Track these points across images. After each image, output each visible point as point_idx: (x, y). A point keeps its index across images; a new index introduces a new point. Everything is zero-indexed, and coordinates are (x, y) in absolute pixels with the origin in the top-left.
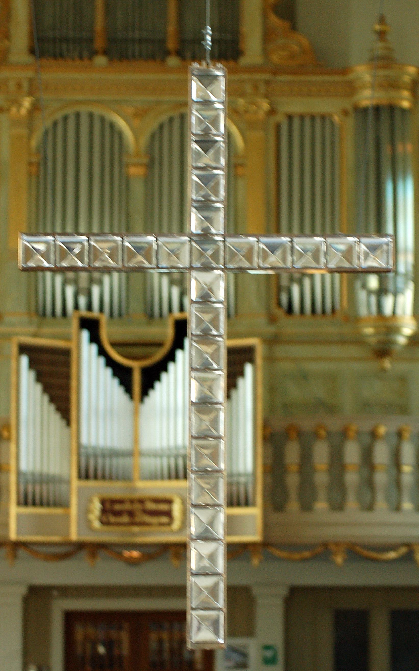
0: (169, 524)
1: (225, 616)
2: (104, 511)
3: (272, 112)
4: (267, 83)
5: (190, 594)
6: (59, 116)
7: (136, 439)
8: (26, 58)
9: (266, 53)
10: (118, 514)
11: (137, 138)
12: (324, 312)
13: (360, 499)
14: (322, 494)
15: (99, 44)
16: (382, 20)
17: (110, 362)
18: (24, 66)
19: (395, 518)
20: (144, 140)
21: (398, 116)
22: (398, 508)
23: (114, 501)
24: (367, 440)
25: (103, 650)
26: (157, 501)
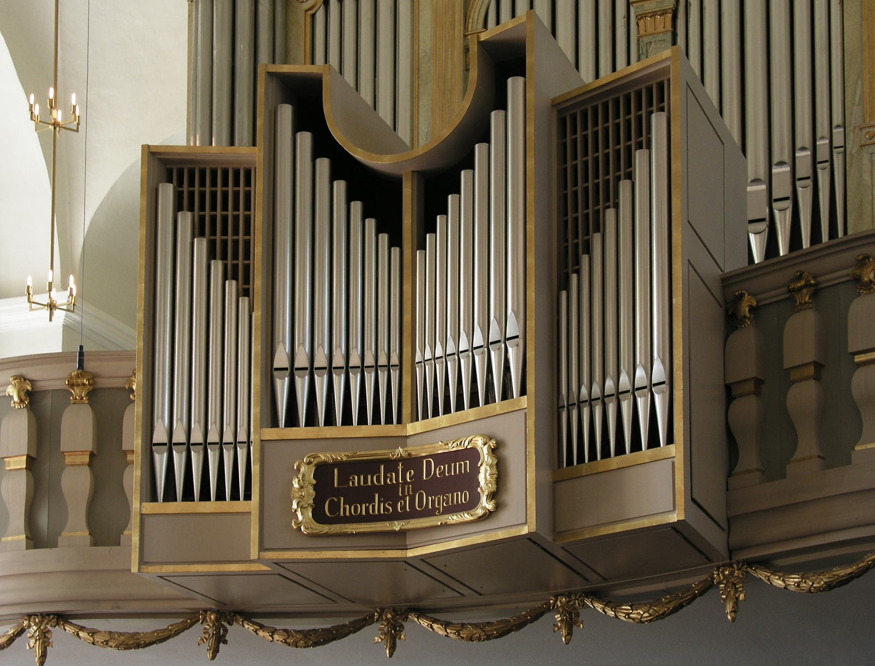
10: (364, 495)
23: (348, 468)
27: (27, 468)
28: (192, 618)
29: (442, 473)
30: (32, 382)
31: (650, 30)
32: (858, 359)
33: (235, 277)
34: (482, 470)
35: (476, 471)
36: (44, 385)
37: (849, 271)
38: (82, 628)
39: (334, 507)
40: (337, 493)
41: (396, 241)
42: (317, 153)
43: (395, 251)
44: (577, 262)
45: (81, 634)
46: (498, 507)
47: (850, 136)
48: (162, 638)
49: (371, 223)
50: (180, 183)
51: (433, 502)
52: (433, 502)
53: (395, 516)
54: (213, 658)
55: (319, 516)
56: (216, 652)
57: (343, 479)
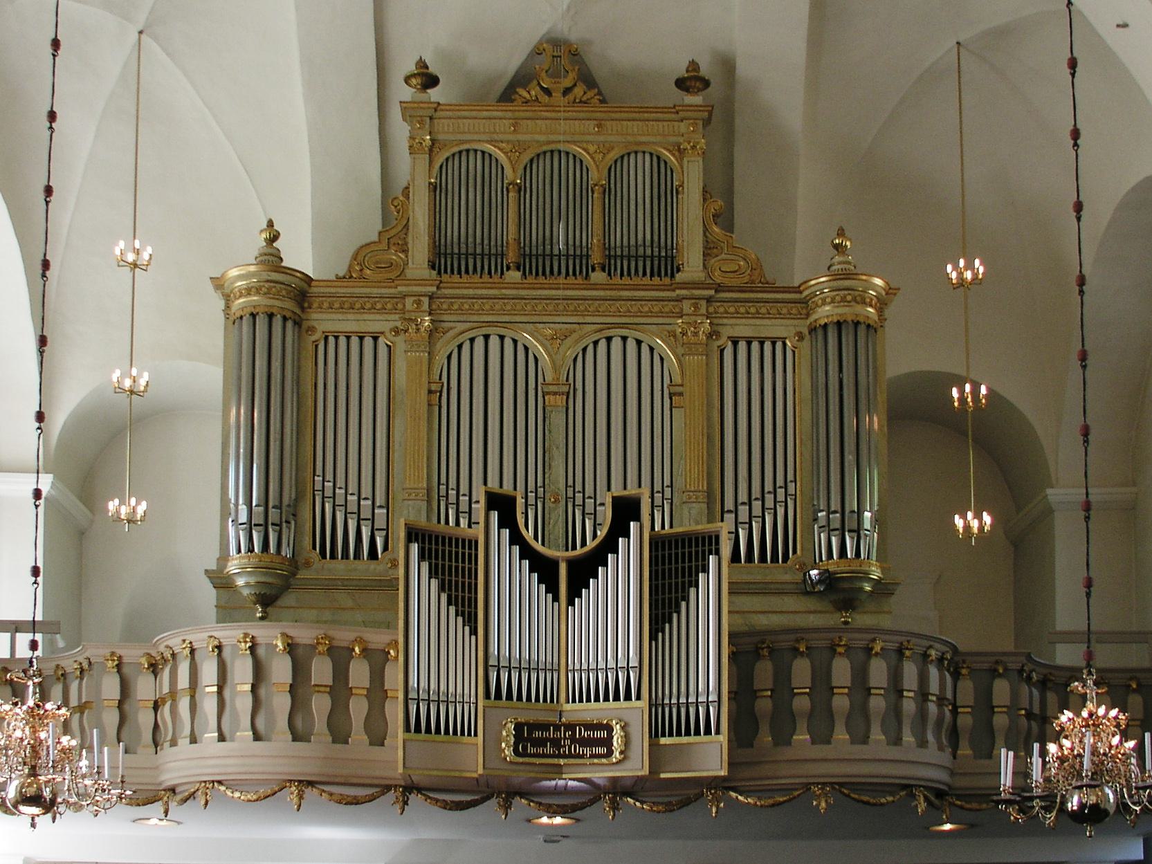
0: (610, 753)
1: (803, 437)
3: (713, 334)
4: (709, 300)
7: (561, 648)
8: (427, 273)
10: (541, 742)
15: (511, 257)
17: (527, 552)
19: (894, 753)
22: (897, 741)
23: (533, 726)
25: (516, 782)
26: (590, 726)
27: (289, 691)
28: (387, 788)
30: (291, 638)
31: (552, 403)
32: (795, 691)
34: (615, 738)
35: (610, 737)
36: (299, 641)
37: (792, 643)
38: (323, 791)
39: (525, 748)
40: (527, 740)
41: (556, 599)
42: (512, 542)
43: (556, 604)
46: (624, 759)
47: (675, 495)
48: (371, 799)
49: (543, 587)
50: (423, 542)
51: (583, 751)
52: (583, 751)
53: (559, 756)
54: (402, 814)
55: (516, 751)
57: (530, 733)
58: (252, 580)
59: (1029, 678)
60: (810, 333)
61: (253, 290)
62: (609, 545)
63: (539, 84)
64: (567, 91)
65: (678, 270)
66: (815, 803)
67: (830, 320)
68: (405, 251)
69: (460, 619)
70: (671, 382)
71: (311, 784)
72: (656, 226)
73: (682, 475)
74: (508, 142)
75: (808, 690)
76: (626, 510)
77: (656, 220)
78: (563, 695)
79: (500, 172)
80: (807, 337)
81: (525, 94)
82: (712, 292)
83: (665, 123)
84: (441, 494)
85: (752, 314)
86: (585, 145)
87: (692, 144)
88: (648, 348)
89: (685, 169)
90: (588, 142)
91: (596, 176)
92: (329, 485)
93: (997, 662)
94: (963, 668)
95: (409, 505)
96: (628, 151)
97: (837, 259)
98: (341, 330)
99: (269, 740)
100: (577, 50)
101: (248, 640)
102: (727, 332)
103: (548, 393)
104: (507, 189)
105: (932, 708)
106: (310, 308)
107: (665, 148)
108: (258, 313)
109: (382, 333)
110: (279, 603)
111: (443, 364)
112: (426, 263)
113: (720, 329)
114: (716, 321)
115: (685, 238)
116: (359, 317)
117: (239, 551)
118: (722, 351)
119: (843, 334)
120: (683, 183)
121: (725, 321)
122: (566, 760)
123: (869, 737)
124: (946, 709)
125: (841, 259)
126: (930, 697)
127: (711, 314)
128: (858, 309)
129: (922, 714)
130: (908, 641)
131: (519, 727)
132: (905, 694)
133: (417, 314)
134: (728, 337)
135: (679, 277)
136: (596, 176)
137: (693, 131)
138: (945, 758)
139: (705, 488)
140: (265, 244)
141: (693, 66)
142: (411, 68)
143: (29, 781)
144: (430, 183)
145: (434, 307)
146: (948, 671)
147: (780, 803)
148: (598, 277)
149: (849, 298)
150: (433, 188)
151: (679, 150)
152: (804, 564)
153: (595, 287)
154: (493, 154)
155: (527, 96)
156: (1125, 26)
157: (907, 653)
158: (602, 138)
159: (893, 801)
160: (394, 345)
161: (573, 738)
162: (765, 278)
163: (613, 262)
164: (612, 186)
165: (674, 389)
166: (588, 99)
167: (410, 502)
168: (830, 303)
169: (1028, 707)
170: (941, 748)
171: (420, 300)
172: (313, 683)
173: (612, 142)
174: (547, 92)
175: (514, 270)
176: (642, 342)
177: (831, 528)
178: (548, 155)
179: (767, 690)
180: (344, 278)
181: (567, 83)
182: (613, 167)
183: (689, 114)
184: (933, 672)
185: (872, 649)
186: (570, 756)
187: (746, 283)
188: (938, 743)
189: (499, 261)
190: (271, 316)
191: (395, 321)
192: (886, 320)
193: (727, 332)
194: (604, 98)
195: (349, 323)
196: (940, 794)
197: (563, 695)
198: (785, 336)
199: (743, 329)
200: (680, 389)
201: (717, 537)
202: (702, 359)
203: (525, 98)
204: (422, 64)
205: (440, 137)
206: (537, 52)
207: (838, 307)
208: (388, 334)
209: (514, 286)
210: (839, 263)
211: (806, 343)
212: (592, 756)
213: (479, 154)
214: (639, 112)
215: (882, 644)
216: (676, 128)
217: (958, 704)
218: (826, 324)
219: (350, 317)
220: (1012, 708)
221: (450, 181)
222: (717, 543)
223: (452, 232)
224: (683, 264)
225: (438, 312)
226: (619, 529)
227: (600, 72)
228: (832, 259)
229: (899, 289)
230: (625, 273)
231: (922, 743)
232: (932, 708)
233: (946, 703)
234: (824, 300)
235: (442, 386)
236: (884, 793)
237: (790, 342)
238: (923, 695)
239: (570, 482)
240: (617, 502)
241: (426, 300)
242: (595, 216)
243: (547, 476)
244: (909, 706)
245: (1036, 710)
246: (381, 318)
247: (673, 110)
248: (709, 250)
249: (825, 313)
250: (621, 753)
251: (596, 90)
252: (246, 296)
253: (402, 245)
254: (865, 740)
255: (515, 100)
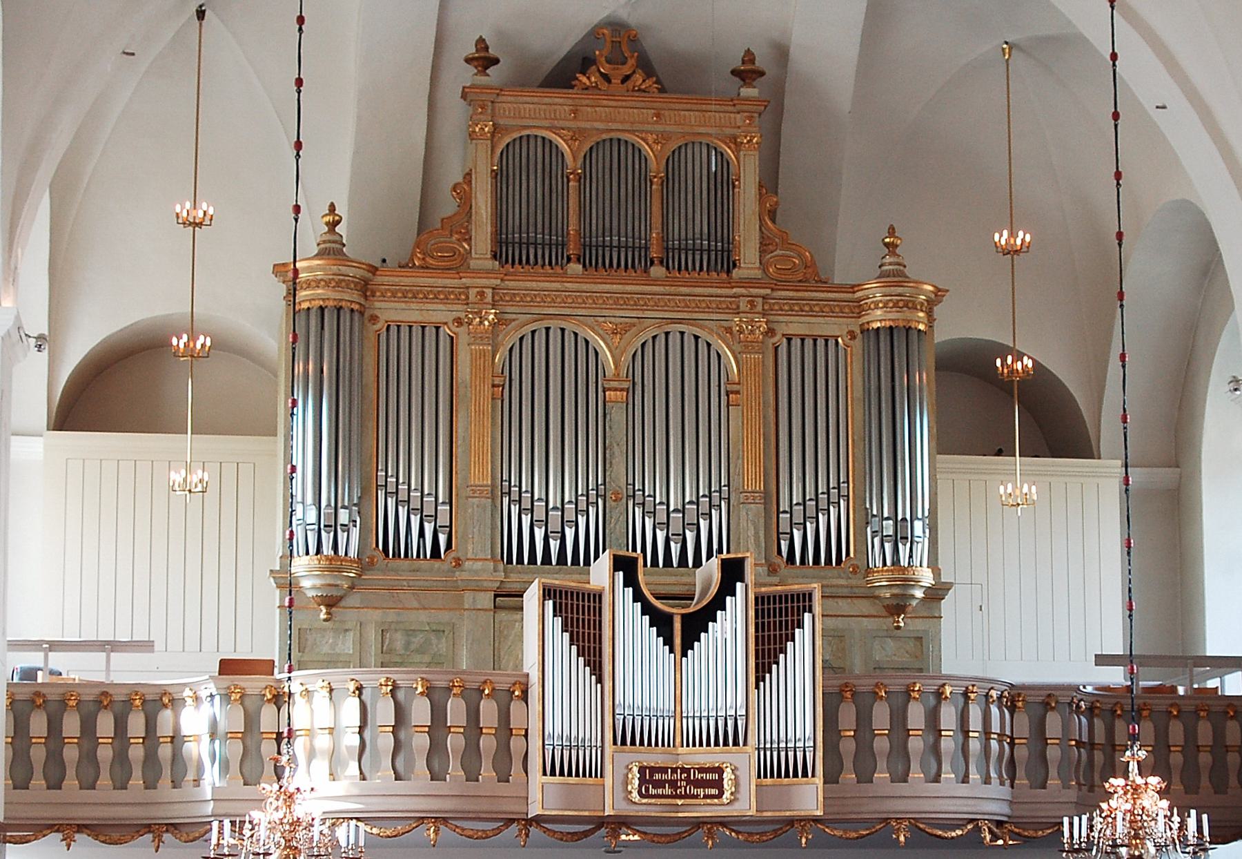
1: (855, 438)
2: (642, 780)
3: (770, 332)
5: (927, 830)
6: (527, 329)
9: (763, 266)
10: (659, 784)
11: (445, 330)
12: (547, 559)
13: (924, 768)
14: (882, 764)
15: (572, 250)
16: (892, 231)
17: (647, 609)
18: (488, 273)
19: (963, 790)
20: (626, 359)
21: (914, 336)
22: (965, 779)
23: (654, 770)
24: (932, 701)
28: (512, 821)
29: (702, 778)
32: (876, 732)
33: (589, 665)
39: (647, 790)
40: (648, 782)
42: (635, 600)
43: (672, 655)
44: (776, 657)
45: (457, 830)
46: (736, 799)
55: (640, 792)
56: (69, 846)
57: (651, 776)
58: (318, 582)
59: (1078, 707)
60: (862, 333)
61: (323, 283)
62: (718, 603)
63: (599, 71)
64: (626, 79)
65: (735, 266)
66: (894, 836)
67: (883, 325)
68: (469, 241)
69: (588, 669)
70: (728, 380)
71: (445, 820)
72: (713, 219)
73: (739, 475)
74: (569, 129)
75: (887, 732)
76: (732, 572)
77: (713, 213)
78: (678, 740)
79: (560, 161)
80: (860, 336)
81: (584, 79)
82: (769, 291)
83: (722, 115)
84: (504, 491)
85: (806, 311)
86: (644, 135)
87: (748, 138)
88: (705, 345)
89: (742, 163)
90: (647, 132)
91: (655, 165)
92: (392, 480)
93: (1049, 696)
94: (1019, 701)
95: (473, 503)
96: (685, 142)
97: (888, 259)
98: (404, 320)
99: (409, 779)
100: (635, 36)
101: (390, 683)
102: (782, 329)
103: (609, 389)
104: (568, 177)
105: (994, 744)
106: (373, 296)
107: (719, 140)
108: (326, 307)
109: (446, 323)
110: (343, 603)
111: (505, 359)
112: (489, 253)
113: (775, 326)
114: (771, 318)
115: (742, 232)
116: (421, 306)
117: (307, 553)
118: (776, 349)
119: (895, 338)
120: (740, 177)
121: (781, 318)
122: (683, 801)
123: (940, 776)
124: (1005, 743)
125: (892, 260)
126: (993, 736)
127: (766, 310)
128: (907, 314)
129: (986, 749)
130: (973, 686)
131: (642, 770)
132: (971, 734)
133: (480, 306)
134: (783, 335)
135: (736, 273)
136: (655, 165)
137: (749, 124)
138: (1005, 792)
139: (762, 488)
140: (326, 229)
141: (749, 57)
142: (471, 50)
143: (285, 853)
144: (493, 171)
145: (497, 298)
146: (1006, 707)
147: (864, 836)
148: (657, 271)
149: (901, 304)
150: (495, 175)
151: (735, 143)
152: (858, 568)
153: (655, 282)
154: (553, 140)
155: (588, 83)
156: (1164, 107)
157: (972, 696)
158: (659, 128)
159: (962, 835)
160: (457, 338)
161: (688, 780)
162: (818, 277)
163: (671, 254)
164: (670, 177)
165: (730, 387)
166: (646, 88)
167: (475, 500)
168: (882, 308)
169: (1077, 738)
170: (1002, 784)
171: (484, 292)
172: (449, 725)
173: (671, 132)
174: (607, 78)
175: (575, 262)
176: (699, 337)
177: (885, 534)
178: (608, 144)
179: (850, 730)
180: (407, 265)
181: (626, 70)
182: (671, 158)
183: (745, 108)
184: (994, 710)
185: (942, 693)
186: (686, 796)
187: (800, 281)
188: (999, 778)
189: (560, 251)
190: (339, 309)
191: (458, 310)
192: (935, 320)
193: (782, 329)
194: (662, 86)
195: (411, 313)
196: (999, 824)
197: (678, 740)
198: (838, 334)
199: (796, 326)
200: (736, 387)
201: (810, 595)
202: (759, 358)
203: (585, 84)
204: (481, 44)
205: (501, 122)
206: (594, 34)
207: (890, 312)
208: (450, 324)
209: (575, 278)
210: (890, 264)
211: (858, 344)
212: (706, 797)
213: (539, 140)
214: (697, 104)
215: (951, 689)
216: (733, 119)
217: (1015, 736)
218: (878, 328)
219: (413, 306)
220: (1065, 737)
221: (511, 166)
222: (810, 600)
223: (513, 220)
224: (739, 260)
225: (501, 303)
226: (727, 588)
227: (653, 56)
228: (883, 258)
229: (947, 291)
230: (683, 268)
231: (987, 780)
232: (994, 744)
233: (1005, 738)
234: (876, 303)
235: (505, 380)
236: (953, 828)
237: (843, 340)
238: (987, 732)
239: (630, 481)
240: (725, 564)
241: (489, 292)
242: (654, 208)
243: (608, 474)
244: (975, 745)
245: (1085, 739)
246: (444, 308)
247: (731, 103)
248: (765, 245)
249: (878, 318)
250: (732, 794)
251: (654, 79)
252: (313, 288)
253: (464, 233)
254: (937, 779)
255: (575, 86)
